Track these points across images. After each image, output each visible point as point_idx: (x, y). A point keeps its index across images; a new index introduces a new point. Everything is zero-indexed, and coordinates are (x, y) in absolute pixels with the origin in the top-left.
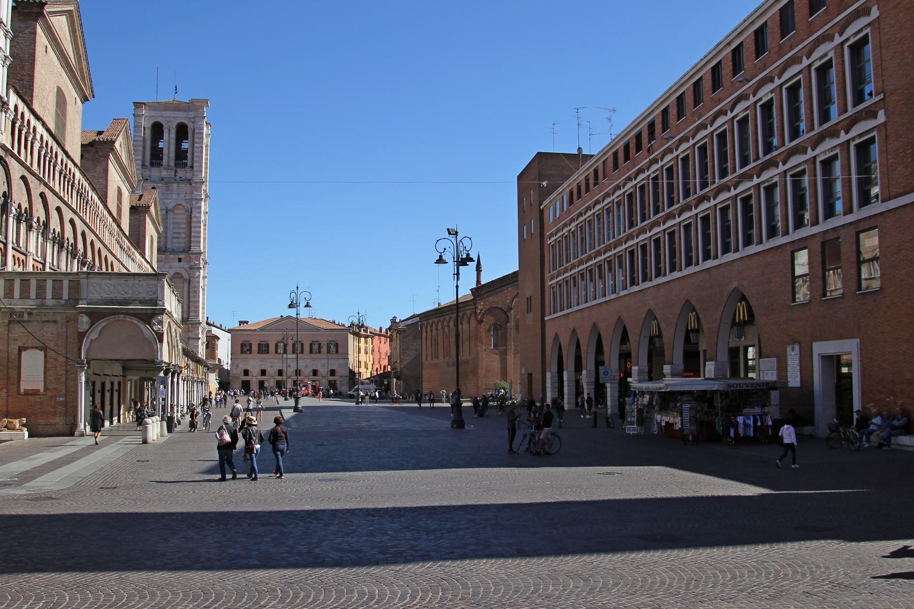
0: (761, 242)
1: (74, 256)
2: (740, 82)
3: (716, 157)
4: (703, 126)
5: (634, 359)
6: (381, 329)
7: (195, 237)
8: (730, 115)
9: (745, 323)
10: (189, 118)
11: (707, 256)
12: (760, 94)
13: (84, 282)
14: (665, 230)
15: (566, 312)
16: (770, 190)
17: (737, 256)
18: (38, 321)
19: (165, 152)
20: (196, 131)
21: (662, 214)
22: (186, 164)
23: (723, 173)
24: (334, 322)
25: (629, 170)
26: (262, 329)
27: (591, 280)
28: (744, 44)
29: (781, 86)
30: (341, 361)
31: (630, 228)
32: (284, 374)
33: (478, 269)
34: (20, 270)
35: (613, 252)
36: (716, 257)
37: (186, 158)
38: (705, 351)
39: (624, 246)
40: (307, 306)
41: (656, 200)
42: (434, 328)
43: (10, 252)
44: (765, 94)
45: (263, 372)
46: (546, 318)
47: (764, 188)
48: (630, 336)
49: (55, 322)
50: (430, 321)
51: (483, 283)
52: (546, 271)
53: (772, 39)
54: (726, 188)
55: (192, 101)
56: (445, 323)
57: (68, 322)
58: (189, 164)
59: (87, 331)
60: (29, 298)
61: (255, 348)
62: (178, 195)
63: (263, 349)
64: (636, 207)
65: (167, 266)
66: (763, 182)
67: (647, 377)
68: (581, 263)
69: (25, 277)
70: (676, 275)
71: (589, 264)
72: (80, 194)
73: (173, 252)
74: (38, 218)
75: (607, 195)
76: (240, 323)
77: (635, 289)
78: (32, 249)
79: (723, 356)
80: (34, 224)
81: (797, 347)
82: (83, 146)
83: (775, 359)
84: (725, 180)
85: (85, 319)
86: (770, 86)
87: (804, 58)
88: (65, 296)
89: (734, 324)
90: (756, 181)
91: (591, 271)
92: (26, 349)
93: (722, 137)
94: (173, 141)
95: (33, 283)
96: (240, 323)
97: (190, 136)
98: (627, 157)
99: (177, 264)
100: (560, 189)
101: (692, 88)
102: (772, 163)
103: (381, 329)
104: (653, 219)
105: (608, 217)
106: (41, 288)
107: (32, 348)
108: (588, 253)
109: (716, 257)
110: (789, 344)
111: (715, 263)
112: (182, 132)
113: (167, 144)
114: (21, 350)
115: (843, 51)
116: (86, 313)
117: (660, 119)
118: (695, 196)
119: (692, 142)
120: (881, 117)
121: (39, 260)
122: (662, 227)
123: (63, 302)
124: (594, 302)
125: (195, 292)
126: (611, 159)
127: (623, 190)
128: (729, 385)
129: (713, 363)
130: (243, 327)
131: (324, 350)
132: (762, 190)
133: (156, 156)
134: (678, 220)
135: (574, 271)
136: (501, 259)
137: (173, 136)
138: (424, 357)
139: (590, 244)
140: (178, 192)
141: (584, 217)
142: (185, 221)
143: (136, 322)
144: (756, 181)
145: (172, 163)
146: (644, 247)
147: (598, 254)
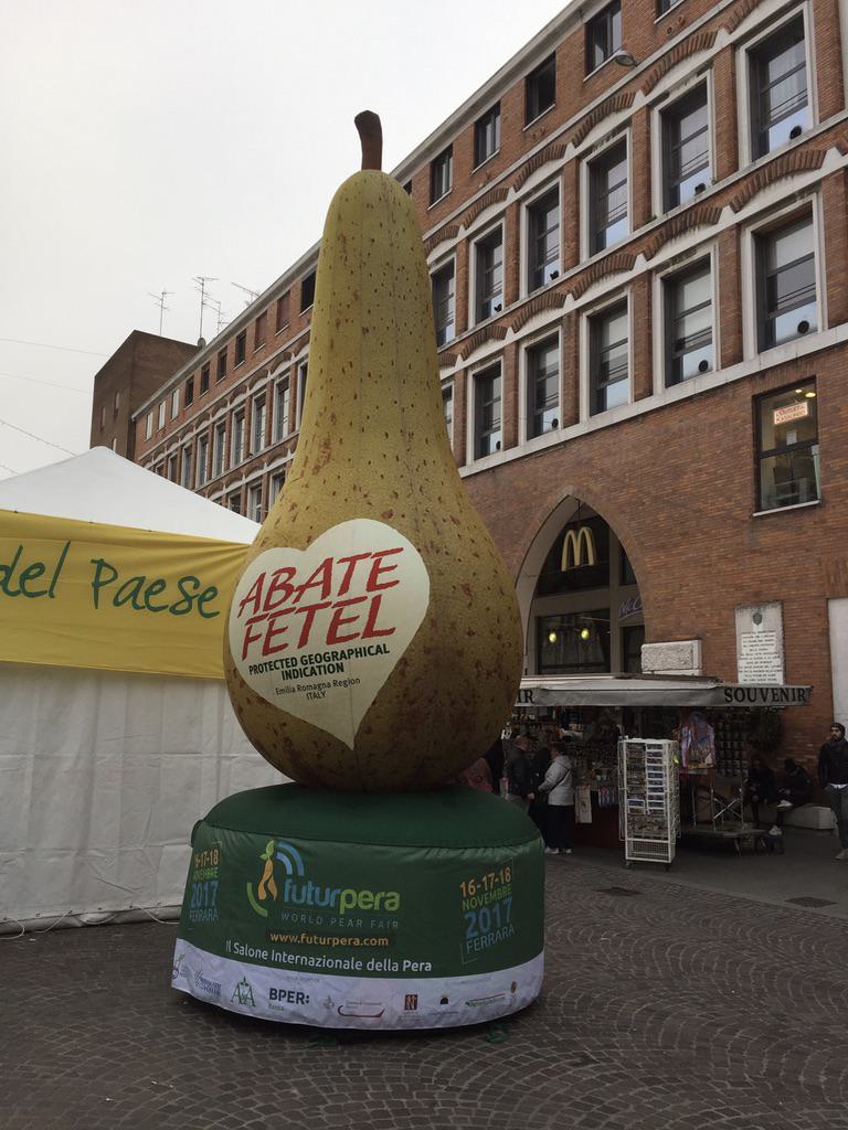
81: (772, 615)
83: (695, 644)
87: (462, 227)
105: (203, 451)
110: (742, 606)
120: (833, 161)
131: (299, 660)
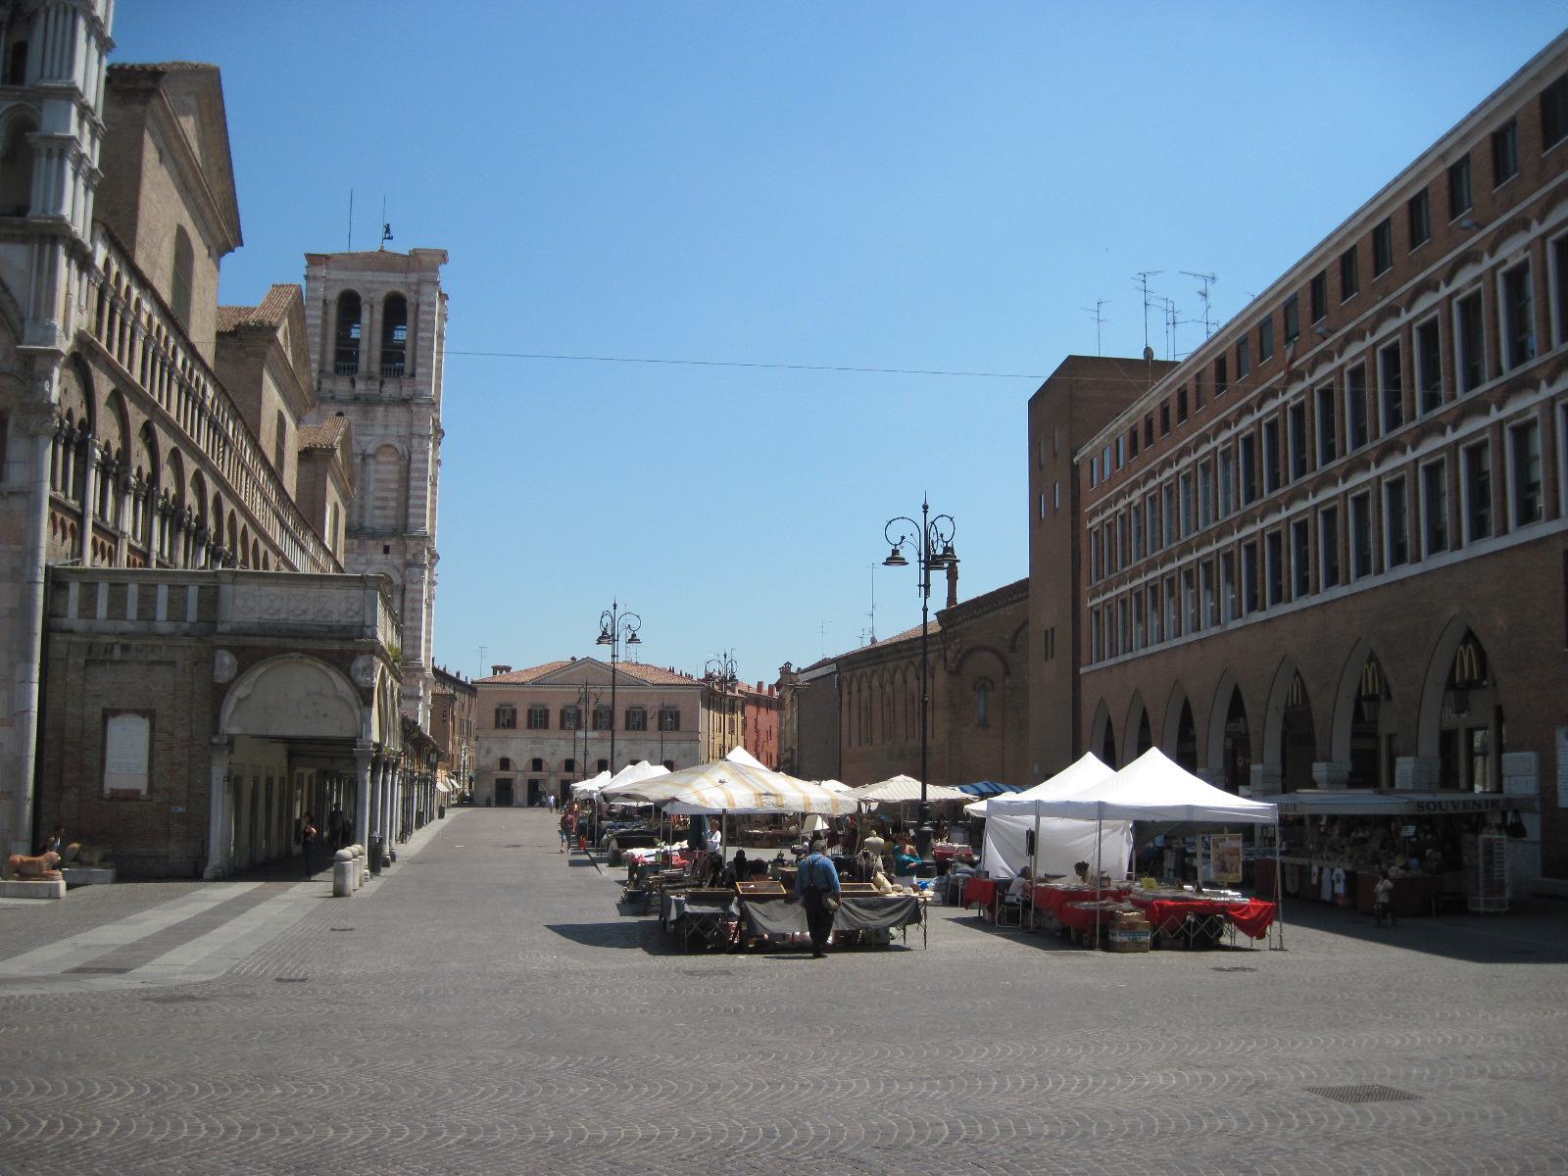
0: (1504, 531)
1: (198, 544)
2: (1465, 228)
3: (1416, 373)
4: (1393, 311)
5: (1254, 754)
6: (760, 685)
7: (416, 506)
8: (1445, 291)
9: (1470, 685)
10: (408, 285)
11: (1399, 558)
12: (1503, 252)
13: (227, 589)
14: (1316, 507)
15: (1121, 659)
16: (1522, 433)
17: (1457, 556)
18: (140, 662)
19: (364, 346)
20: (423, 308)
21: (1286, 489)
22: (401, 371)
23: (1432, 401)
24: (672, 671)
25: (1246, 392)
26: (537, 683)
27: (1209, 585)
28: (1358, 249)
29: (1544, 237)
30: (686, 746)
31: (1247, 502)
32: (576, 768)
33: (952, 577)
34: (104, 565)
35: (1215, 546)
36: (1417, 559)
37: (402, 359)
38: (1390, 737)
39: (1237, 536)
40: (633, 639)
41: (1393, 398)
42: (864, 686)
43: (89, 534)
44: (1513, 250)
45: (537, 764)
46: (1082, 671)
47: (1323, 512)
48: (1247, 707)
49: (172, 663)
50: (858, 672)
51: (960, 600)
52: (1084, 580)
53: (1526, 149)
54: (1437, 428)
55: (415, 254)
56: (887, 677)
57: (195, 664)
58: (408, 369)
59: (231, 682)
60: (124, 617)
61: (522, 718)
62: (386, 427)
63: (538, 719)
64: (1265, 460)
65: (362, 560)
66: (1509, 419)
67: (1279, 786)
68: (1152, 566)
69: (118, 584)
70: (1339, 591)
71: (1166, 569)
72: (214, 426)
73: (374, 535)
74: (140, 469)
75: (1204, 439)
76: (496, 669)
77: (1258, 616)
78: (128, 527)
79: (1429, 746)
80: (133, 480)
82: (220, 335)
84: (1437, 412)
85: (226, 659)
86: (1521, 240)
88: (192, 615)
89: (1451, 685)
90: (1495, 415)
91: (1138, 595)
92: (116, 713)
93: (1429, 332)
94: (378, 327)
95: (133, 590)
96: (496, 669)
97: (410, 317)
98: (1183, 413)
99: (380, 556)
100: (1113, 427)
101: (1370, 238)
102: (1527, 383)
103: (760, 685)
104: (1293, 484)
105: (1206, 482)
106: (147, 600)
107: (127, 711)
108: (1166, 547)
109: (1380, 570)
111: (1457, 556)
112: (396, 309)
113: (367, 331)
114: (108, 714)
115: (1342, 374)
116: (229, 648)
117: (1309, 295)
118: (1376, 443)
119: (1370, 340)
121: (140, 545)
122: (1312, 501)
123: (186, 626)
124: (1176, 642)
125: (413, 610)
126: (1212, 371)
127: (1234, 430)
128: (1420, 805)
129: (1412, 759)
130: (500, 677)
132: (1350, 502)
133: (346, 357)
134: (1342, 487)
135: (1137, 582)
136: (997, 555)
137: (379, 316)
138: (845, 740)
139: (1153, 541)
140: (386, 425)
141: (1159, 480)
142: (397, 477)
143: (324, 669)
144: (1495, 415)
145: (376, 368)
146: (1275, 538)
147: (1186, 549)
